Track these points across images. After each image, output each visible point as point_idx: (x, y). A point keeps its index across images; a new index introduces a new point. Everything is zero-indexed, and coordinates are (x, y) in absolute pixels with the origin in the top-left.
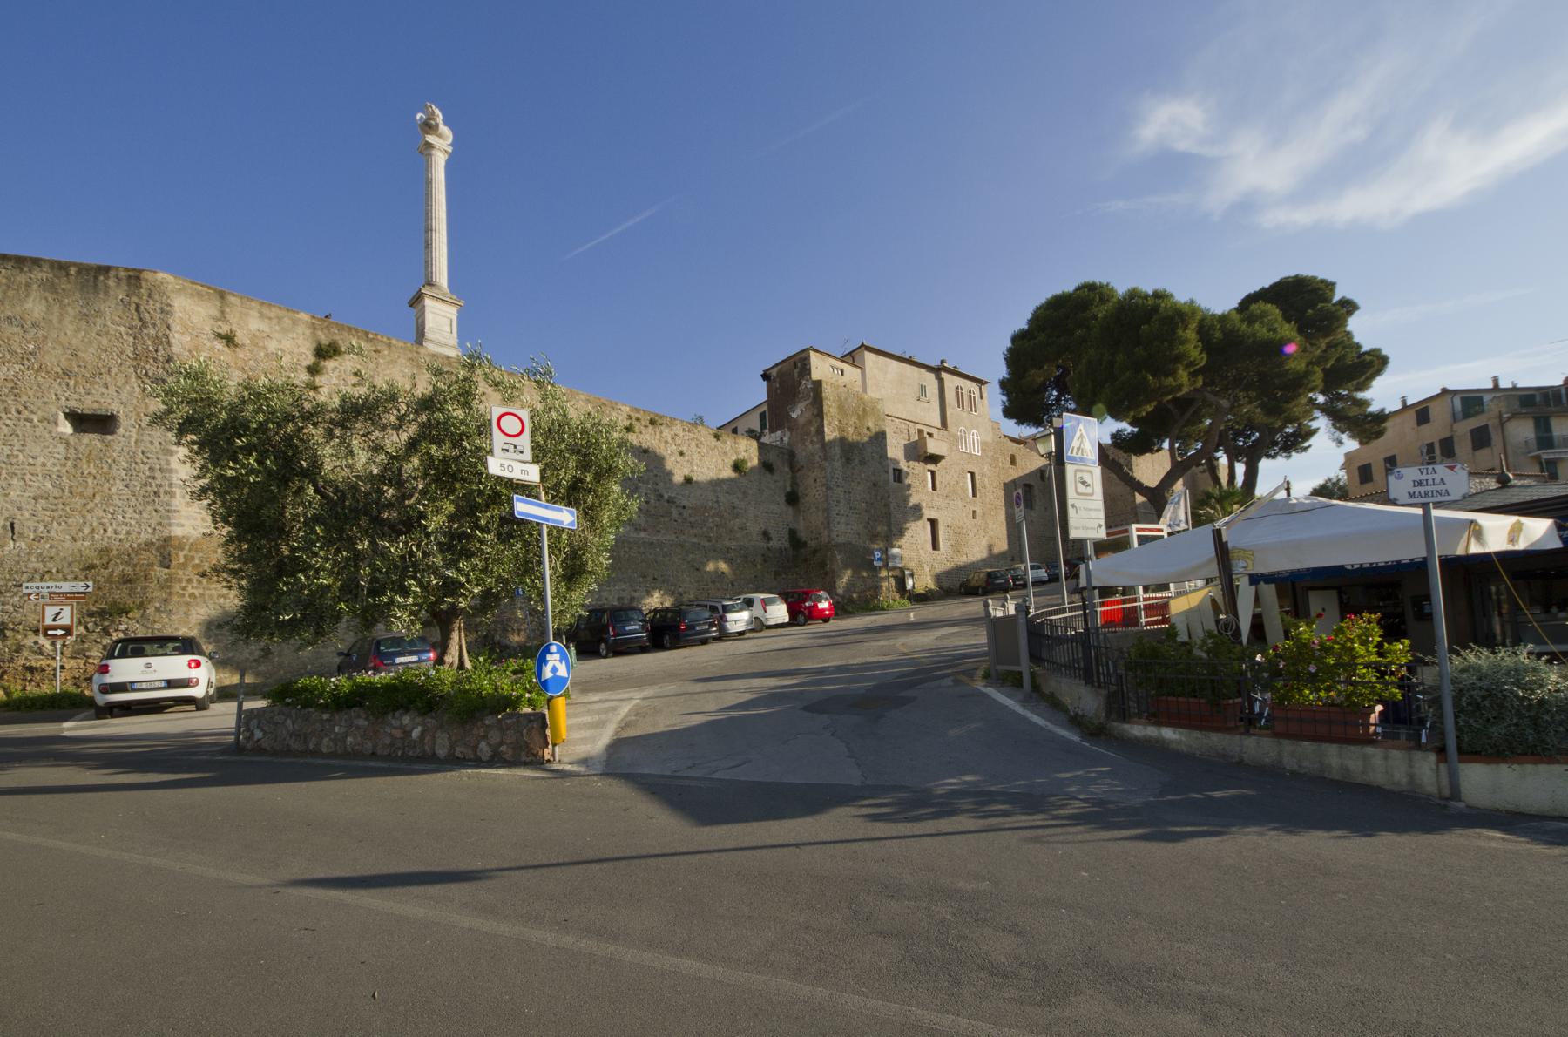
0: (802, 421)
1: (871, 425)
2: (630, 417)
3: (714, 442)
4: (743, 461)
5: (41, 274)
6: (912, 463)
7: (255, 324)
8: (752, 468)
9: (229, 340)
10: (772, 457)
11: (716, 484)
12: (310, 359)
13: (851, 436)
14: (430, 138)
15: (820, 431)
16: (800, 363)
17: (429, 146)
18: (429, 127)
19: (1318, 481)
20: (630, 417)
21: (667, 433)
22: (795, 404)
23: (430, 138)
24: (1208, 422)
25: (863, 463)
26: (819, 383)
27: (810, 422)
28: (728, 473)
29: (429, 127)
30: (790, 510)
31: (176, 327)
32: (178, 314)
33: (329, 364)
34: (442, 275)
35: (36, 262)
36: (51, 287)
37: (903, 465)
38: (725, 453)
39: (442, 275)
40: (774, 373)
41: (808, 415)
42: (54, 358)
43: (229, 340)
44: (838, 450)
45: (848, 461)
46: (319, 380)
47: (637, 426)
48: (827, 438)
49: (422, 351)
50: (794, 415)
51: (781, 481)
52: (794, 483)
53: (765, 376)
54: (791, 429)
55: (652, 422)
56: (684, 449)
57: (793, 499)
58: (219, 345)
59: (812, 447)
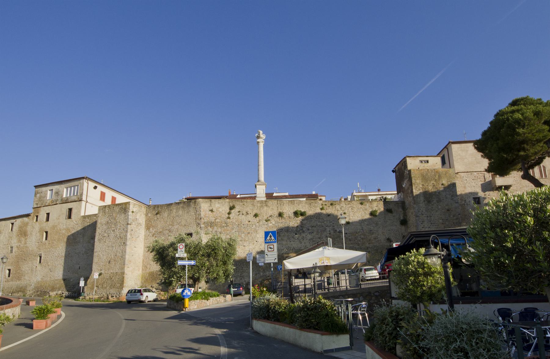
0: (406, 188)
1: (444, 182)
2: (322, 205)
3: (360, 206)
4: (376, 211)
5: (181, 205)
6: (487, 193)
7: (217, 205)
8: (381, 213)
9: (212, 211)
10: (391, 206)
11: (362, 222)
12: (228, 211)
13: (431, 189)
14: (258, 140)
15: (412, 192)
16: (403, 163)
17: (258, 142)
18: (258, 137)
19: (510, 101)
20: (322, 205)
21: (338, 207)
22: (403, 181)
23: (258, 140)
24: (514, 258)
25: (439, 201)
26: (410, 171)
27: (408, 188)
28: (367, 216)
29: (258, 137)
30: (403, 228)
31: (202, 211)
32: (202, 207)
33: (233, 211)
34: (262, 178)
35: (171, 204)
36: (183, 207)
37: (481, 194)
38: (366, 209)
39: (262, 178)
40: (121, 218)
41: (408, 185)
42: (183, 223)
43: (212, 211)
44: (422, 199)
45: (429, 202)
46: (230, 216)
47: (325, 207)
48: (414, 194)
49: (255, 201)
50: (404, 186)
51: (399, 214)
52: (405, 215)
53: (393, 171)
54: (403, 192)
55: (332, 204)
56: (346, 211)
57: (404, 222)
58: (210, 213)
59: (410, 199)
